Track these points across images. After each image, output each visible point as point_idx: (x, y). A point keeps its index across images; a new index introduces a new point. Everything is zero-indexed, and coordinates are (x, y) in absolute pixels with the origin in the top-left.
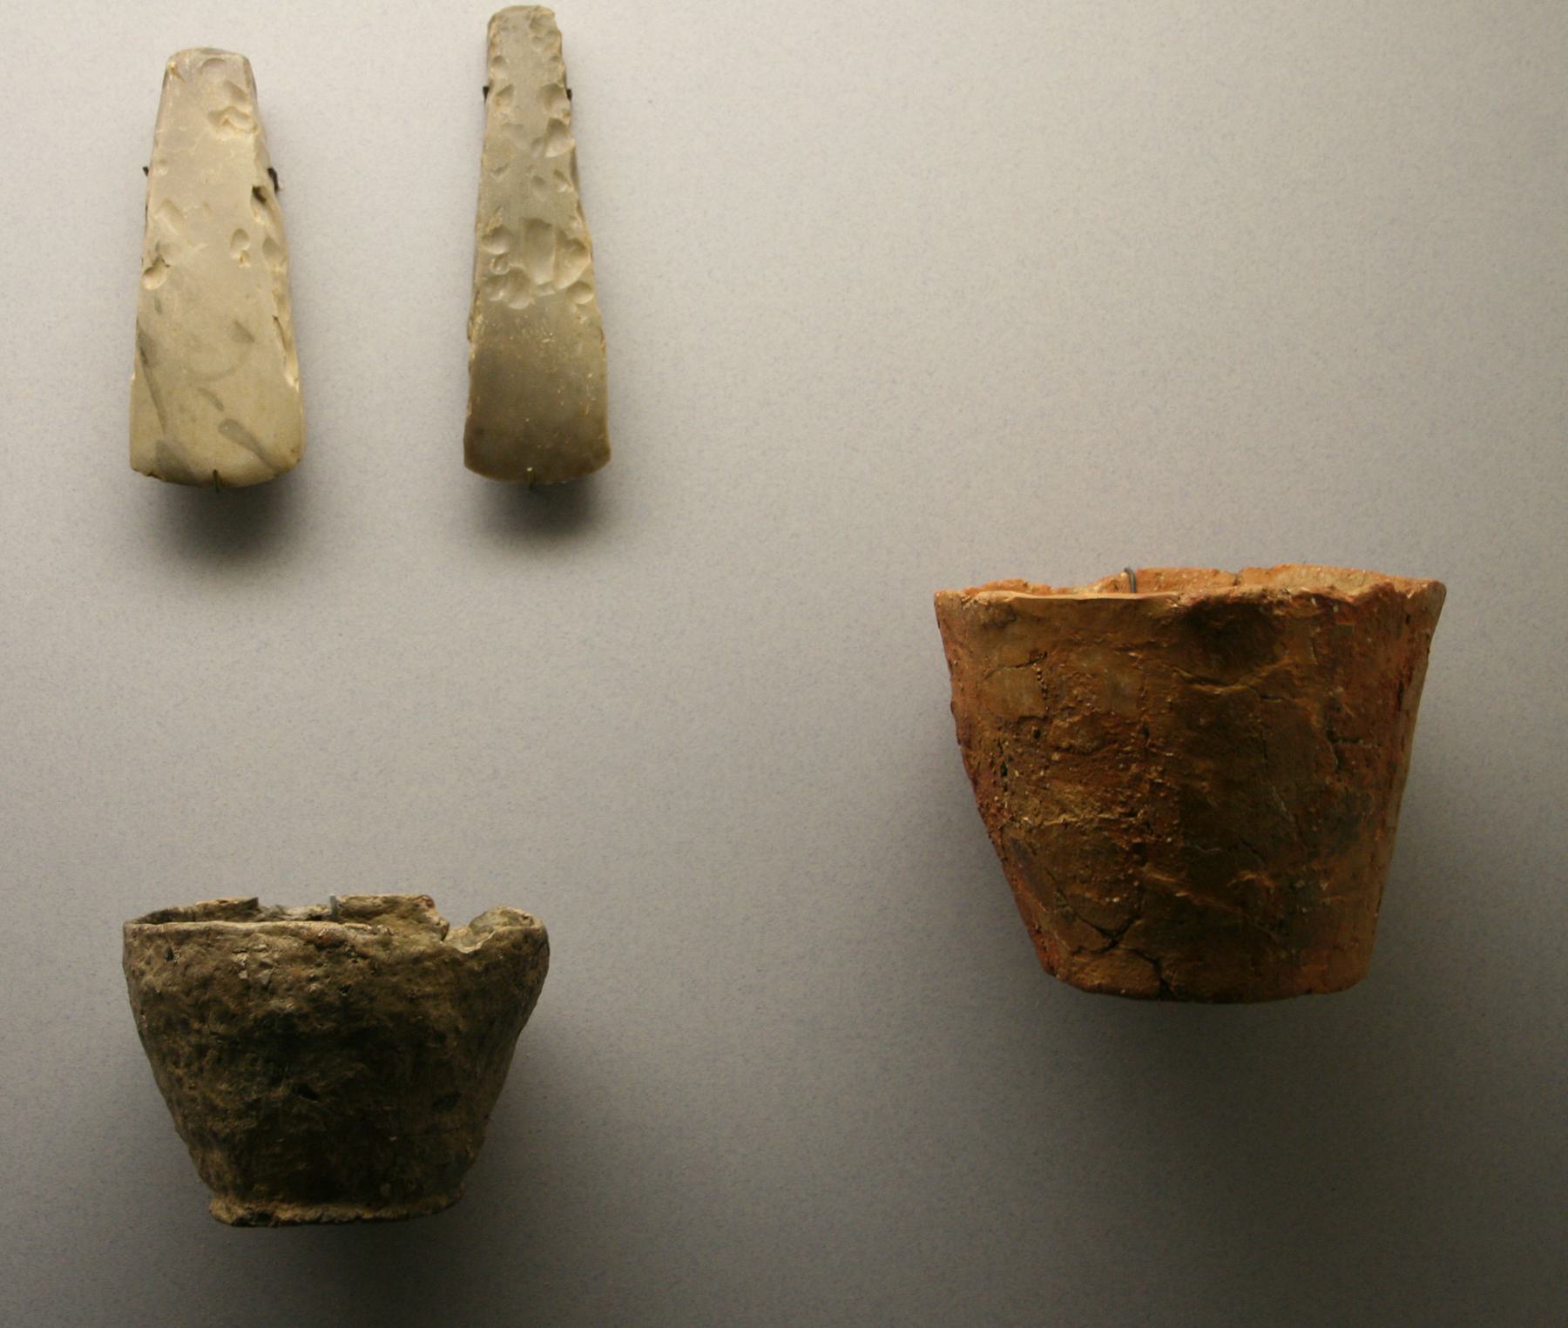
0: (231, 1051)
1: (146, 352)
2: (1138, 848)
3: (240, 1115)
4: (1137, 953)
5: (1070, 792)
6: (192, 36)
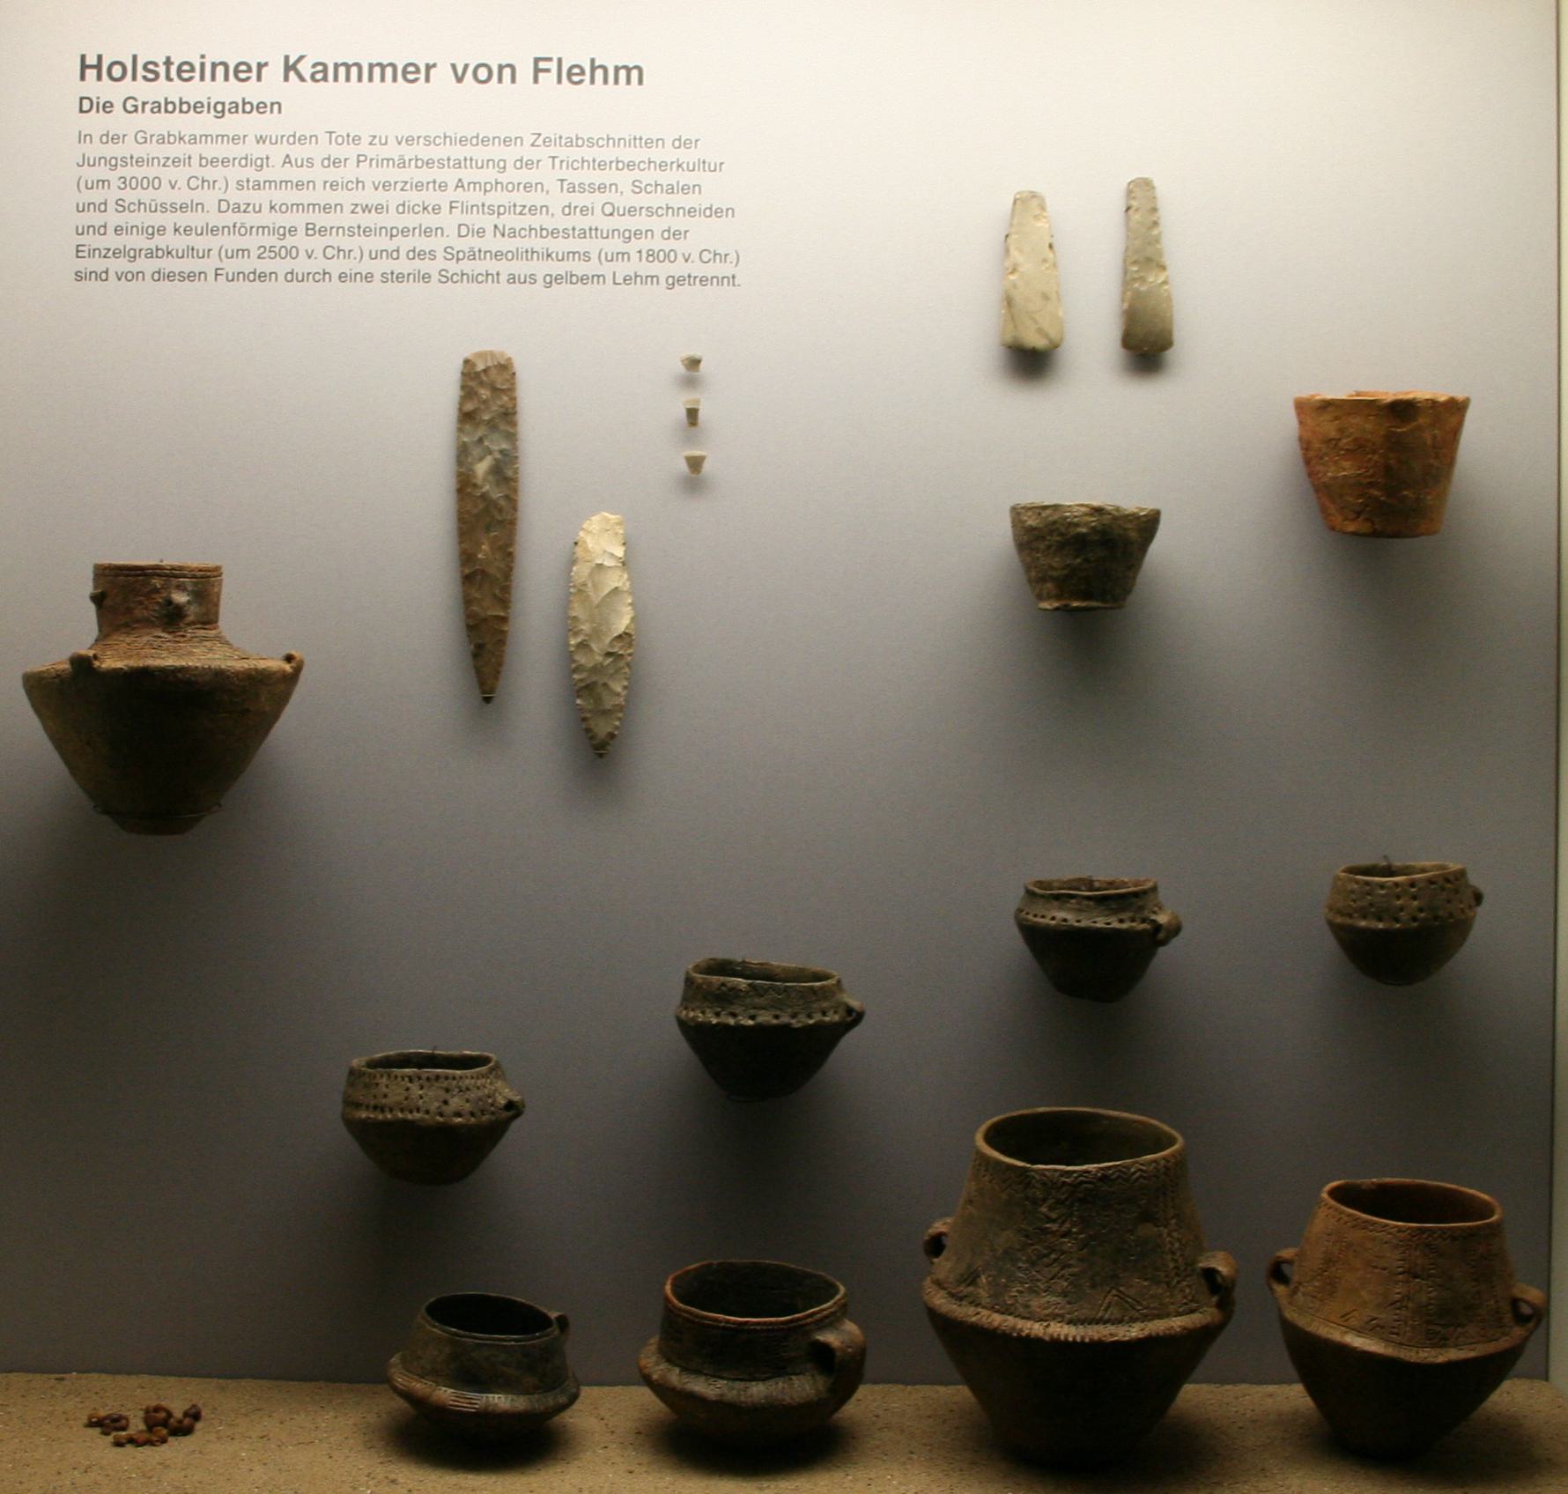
0: (1061, 547)
1: (1009, 302)
2: (1370, 483)
3: (1063, 569)
4: (1367, 519)
5: (1346, 464)
6: (1027, 187)
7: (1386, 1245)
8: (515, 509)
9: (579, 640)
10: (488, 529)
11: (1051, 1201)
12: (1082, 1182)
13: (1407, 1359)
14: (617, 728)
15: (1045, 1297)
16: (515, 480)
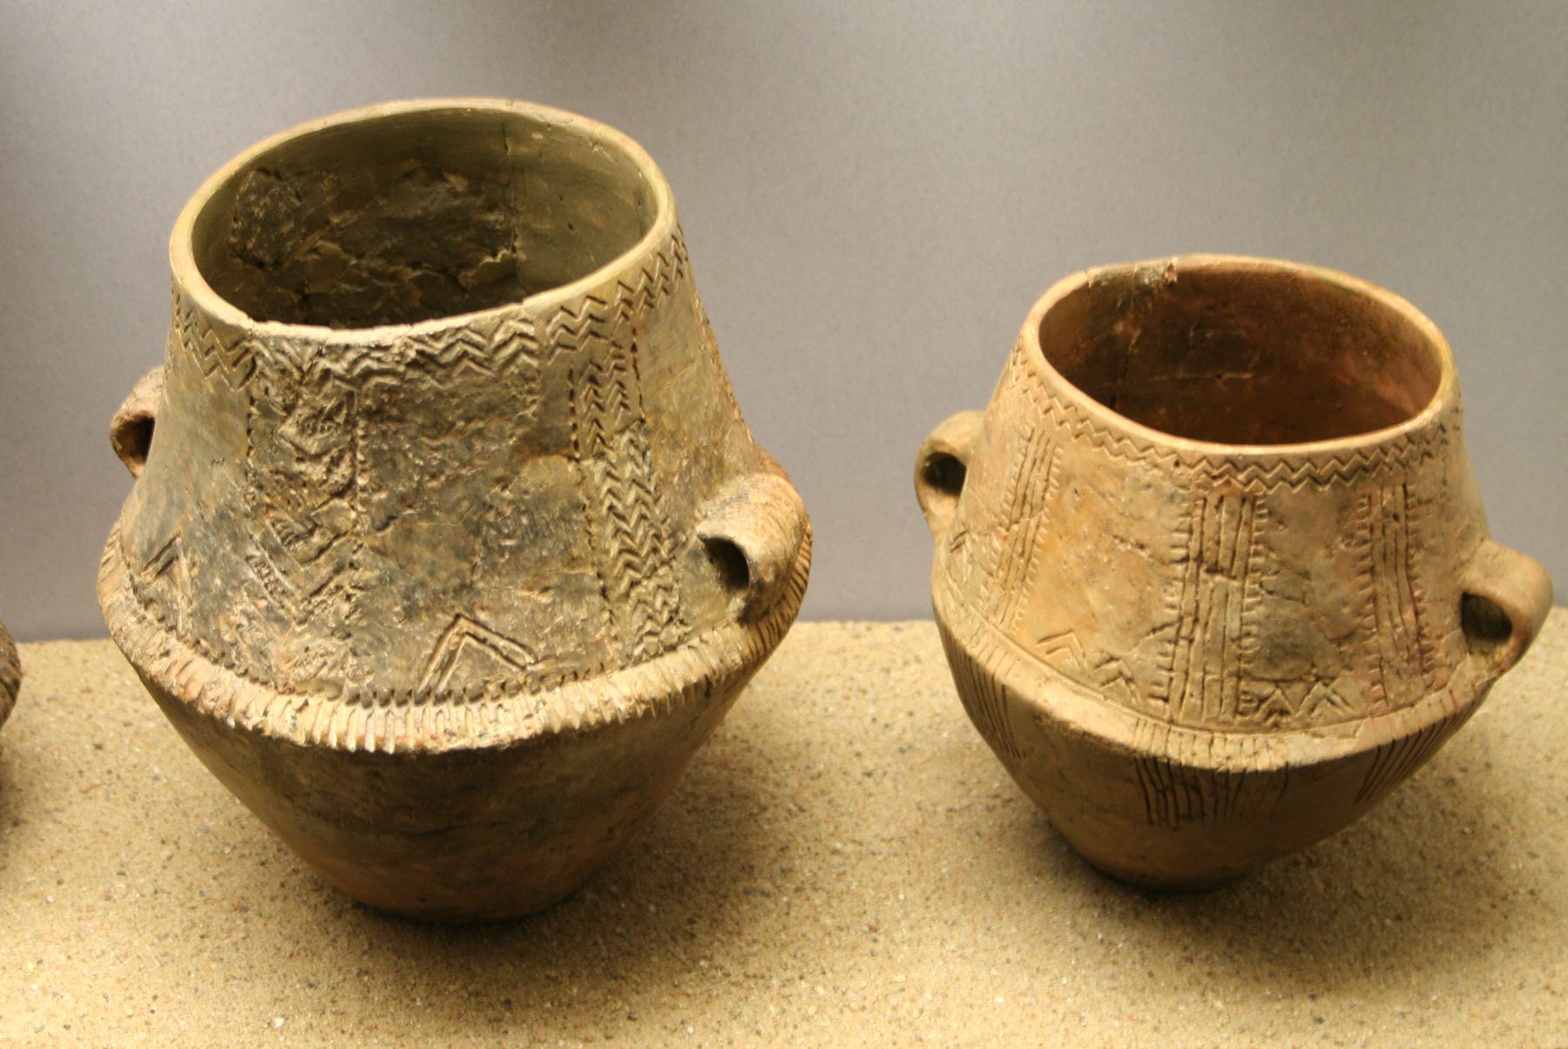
7: (1144, 493)
11: (302, 412)
12: (368, 374)
13: (1184, 759)
15: (301, 634)
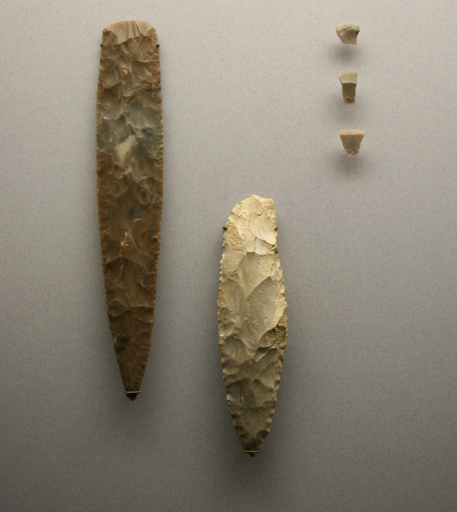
8: (160, 193)
9: (229, 333)
10: (131, 215)
14: (269, 425)
16: (160, 162)
